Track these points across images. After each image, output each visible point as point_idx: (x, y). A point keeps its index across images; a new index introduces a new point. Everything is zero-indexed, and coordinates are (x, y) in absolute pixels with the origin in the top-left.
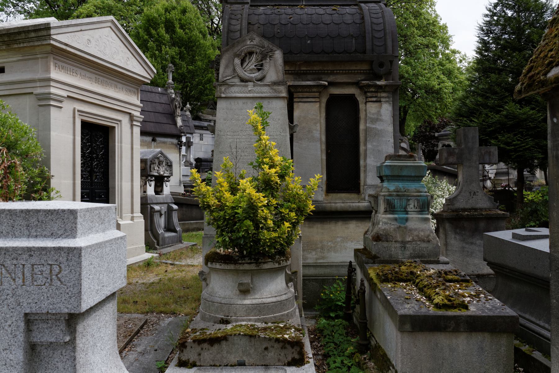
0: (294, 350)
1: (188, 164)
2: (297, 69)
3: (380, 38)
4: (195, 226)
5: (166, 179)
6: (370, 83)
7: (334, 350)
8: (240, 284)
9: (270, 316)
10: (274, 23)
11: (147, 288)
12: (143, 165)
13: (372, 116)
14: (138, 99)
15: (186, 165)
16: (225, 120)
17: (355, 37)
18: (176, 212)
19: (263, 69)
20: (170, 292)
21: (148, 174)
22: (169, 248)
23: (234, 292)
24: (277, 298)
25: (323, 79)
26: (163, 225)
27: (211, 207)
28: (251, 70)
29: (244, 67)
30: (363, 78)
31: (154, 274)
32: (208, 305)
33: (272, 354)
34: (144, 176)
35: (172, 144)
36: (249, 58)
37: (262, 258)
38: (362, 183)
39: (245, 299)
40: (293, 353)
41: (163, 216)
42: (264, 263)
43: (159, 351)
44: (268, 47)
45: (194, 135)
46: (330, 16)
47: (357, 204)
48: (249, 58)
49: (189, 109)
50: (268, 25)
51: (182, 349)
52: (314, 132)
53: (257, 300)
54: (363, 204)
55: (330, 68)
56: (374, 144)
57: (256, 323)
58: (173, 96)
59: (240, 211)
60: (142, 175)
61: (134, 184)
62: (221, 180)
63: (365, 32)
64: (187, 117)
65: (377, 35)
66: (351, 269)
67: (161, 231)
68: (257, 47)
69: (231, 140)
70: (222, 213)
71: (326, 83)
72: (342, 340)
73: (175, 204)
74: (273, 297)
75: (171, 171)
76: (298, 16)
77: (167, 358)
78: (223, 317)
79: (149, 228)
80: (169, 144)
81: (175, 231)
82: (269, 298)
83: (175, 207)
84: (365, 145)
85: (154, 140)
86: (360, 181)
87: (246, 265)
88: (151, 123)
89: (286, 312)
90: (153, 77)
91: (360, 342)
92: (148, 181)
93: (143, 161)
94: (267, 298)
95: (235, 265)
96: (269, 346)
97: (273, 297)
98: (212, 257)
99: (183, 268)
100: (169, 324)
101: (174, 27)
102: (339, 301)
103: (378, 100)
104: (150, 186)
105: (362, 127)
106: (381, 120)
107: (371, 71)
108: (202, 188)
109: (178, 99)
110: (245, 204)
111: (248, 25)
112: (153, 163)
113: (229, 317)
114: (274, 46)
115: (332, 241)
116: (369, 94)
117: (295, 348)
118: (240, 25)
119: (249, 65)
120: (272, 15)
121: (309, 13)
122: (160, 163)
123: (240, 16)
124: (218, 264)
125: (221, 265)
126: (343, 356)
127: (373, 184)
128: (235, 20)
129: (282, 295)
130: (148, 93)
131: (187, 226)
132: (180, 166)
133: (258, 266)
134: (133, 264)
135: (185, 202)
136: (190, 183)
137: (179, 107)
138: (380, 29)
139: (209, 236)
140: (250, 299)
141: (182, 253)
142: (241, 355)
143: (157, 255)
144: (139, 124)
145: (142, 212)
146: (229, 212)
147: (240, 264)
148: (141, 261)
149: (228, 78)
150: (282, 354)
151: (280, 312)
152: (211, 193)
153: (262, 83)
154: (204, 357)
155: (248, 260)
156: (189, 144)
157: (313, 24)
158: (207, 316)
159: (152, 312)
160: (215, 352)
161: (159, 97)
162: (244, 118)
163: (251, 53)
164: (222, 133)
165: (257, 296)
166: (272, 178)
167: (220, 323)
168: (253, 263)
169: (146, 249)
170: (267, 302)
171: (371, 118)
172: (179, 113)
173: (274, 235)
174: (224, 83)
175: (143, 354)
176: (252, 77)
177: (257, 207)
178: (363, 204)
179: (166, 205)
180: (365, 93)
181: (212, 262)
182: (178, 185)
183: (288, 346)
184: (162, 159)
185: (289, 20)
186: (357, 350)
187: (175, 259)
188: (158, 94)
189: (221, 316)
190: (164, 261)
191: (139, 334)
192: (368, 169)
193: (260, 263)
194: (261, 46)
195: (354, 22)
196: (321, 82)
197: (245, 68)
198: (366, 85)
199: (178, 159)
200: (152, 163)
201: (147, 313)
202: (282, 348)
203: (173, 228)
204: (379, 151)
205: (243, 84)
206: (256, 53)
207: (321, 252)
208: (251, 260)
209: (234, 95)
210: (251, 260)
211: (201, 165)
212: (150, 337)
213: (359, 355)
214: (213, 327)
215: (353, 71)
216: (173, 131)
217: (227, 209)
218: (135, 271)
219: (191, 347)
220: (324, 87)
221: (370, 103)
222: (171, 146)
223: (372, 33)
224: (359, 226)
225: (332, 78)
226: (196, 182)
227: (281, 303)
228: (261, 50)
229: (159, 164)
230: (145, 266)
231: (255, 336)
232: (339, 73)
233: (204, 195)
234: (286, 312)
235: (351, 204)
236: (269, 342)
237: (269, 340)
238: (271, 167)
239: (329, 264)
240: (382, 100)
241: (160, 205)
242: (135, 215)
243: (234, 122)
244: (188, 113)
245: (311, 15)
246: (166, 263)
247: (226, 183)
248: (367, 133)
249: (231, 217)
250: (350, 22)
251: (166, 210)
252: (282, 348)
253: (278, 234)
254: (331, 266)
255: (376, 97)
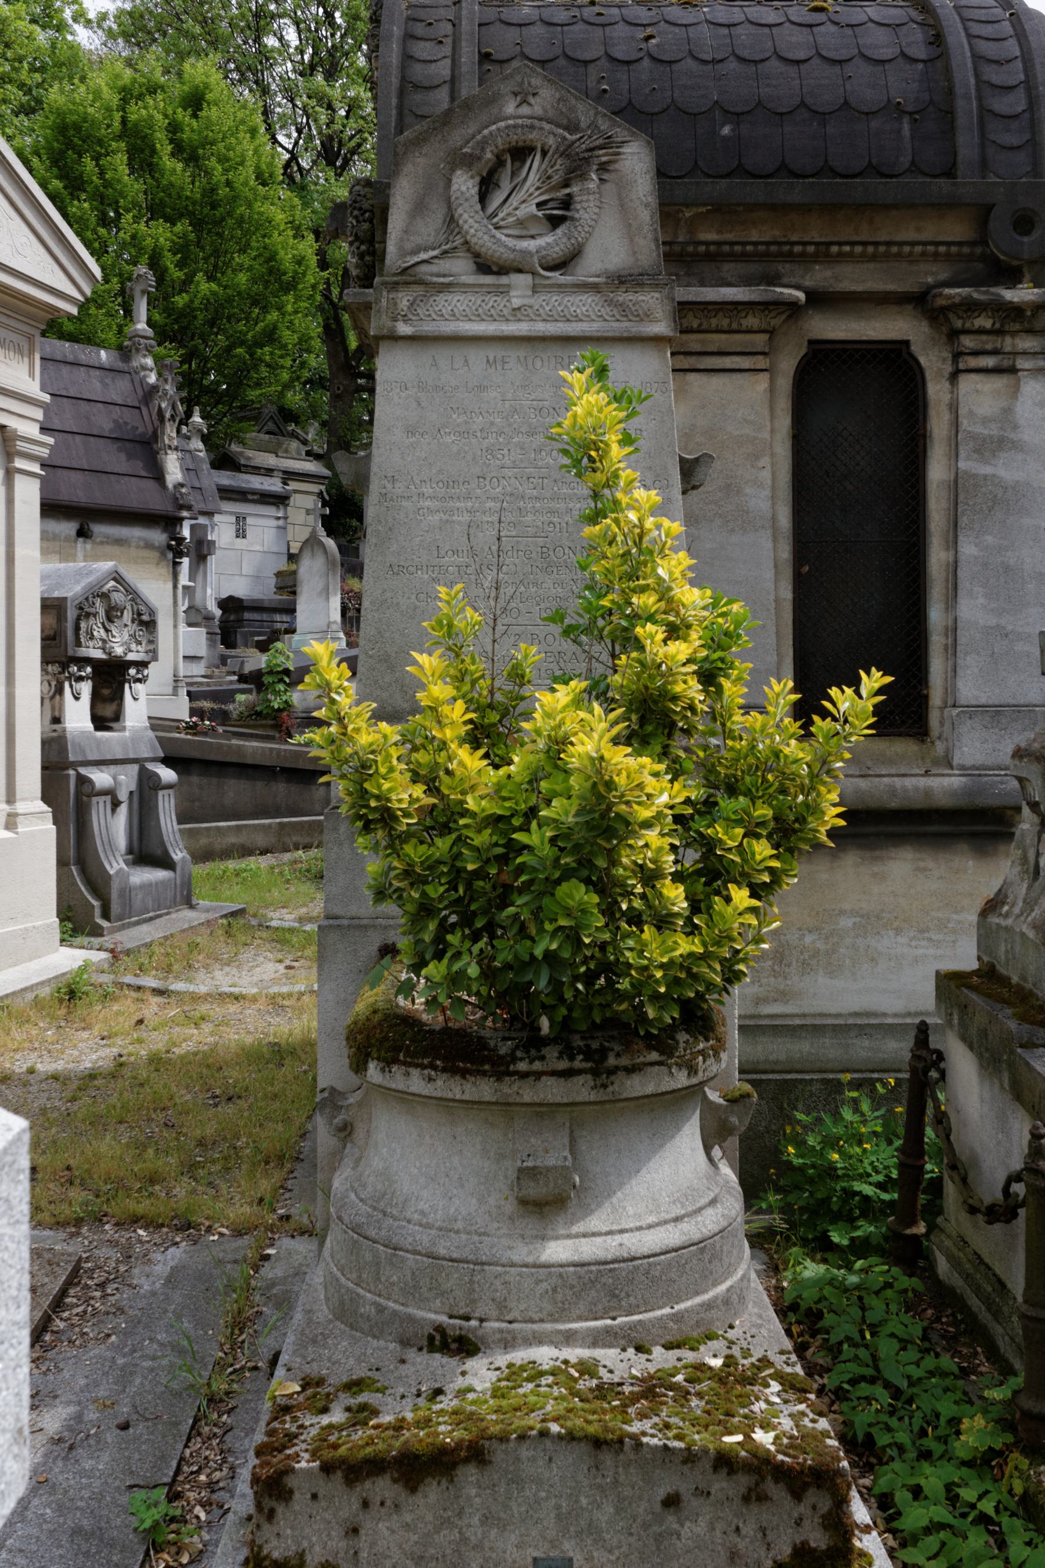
0: (803, 1509)
1: (199, 619)
2: (681, 239)
3: (1016, 117)
4: (232, 840)
5: (132, 671)
6: (975, 295)
7: (894, 1422)
8: (527, 1174)
9: (659, 1313)
10: (587, 56)
11: (73, 1100)
12: (52, 620)
13: (978, 429)
14: (31, 374)
15: (193, 620)
16: (410, 431)
17: (911, 114)
18: (171, 791)
19: (573, 219)
20: (160, 1117)
21: (70, 653)
22: (145, 928)
23: (492, 1201)
24: (684, 1226)
25: (785, 280)
26: (121, 841)
27: (396, 819)
28: (521, 223)
29: (490, 210)
30: (943, 276)
31: (96, 1031)
32: (368, 1257)
33: (701, 1528)
34: (53, 663)
35: (149, 546)
36: (514, 174)
37: (617, 1048)
38: (936, 697)
39: (544, 1238)
40: (799, 1522)
41: (123, 809)
42: (630, 1070)
43: (139, 1429)
44: (593, 125)
45: (217, 518)
46: (806, 30)
47: (923, 782)
48: (514, 174)
49: (200, 431)
50: (562, 62)
51: (268, 1503)
52: (748, 491)
53: (599, 1240)
54: (946, 781)
55: (816, 232)
56: (989, 539)
57: (599, 1353)
58: (152, 379)
59: (535, 838)
60: (46, 660)
61: (19, 692)
62: (440, 691)
63: (950, 91)
64: (194, 458)
65: (1002, 104)
66: (924, 1053)
67: (116, 865)
68: (547, 127)
69: (437, 517)
70: (443, 844)
71: (801, 296)
72: (916, 1373)
73: (168, 761)
74: (666, 1222)
75: (150, 642)
76: (677, 30)
77: (174, 1463)
78: (443, 1319)
79: (72, 853)
80: (138, 547)
81: (165, 862)
82: (650, 1227)
83: (167, 774)
84: (953, 542)
85: (82, 533)
86: (927, 687)
87: (550, 1081)
88: (72, 473)
89: (722, 1288)
90: (88, 292)
91: (1028, 1403)
92: (69, 679)
93: (51, 607)
94: (639, 1229)
95: (499, 1080)
96: (685, 1489)
97: (666, 1222)
98: (386, 1039)
99: (204, 1008)
100: (171, 1280)
101: (154, 151)
102: (864, 1176)
103: (1006, 363)
104: (77, 698)
105: (937, 472)
106: (1017, 446)
107: (979, 250)
108: (357, 730)
109: (170, 388)
110: (574, 806)
111: (480, 63)
112: (88, 615)
113: (474, 1323)
114: (615, 124)
115: (818, 929)
116: (968, 342)
117: (812, 1496)
118: (448, 61)
119: (514, 201)
120: (576, 28)
121: (721, 21)
122: (112, 614)
123: (449, 26)
124: (415, 1072)
125: (430, 1079)
126: (947, 1456)
127: (983, 700)
128: (428, 44)
129: (700, 1210)
130: (62, 366)
131: (204, 841)
132: (175, 626)
133: (604, 1086)
134: (14, 993)
135: (196, 754)
136: (208, 684)
137: (173, 418)
138: (1011, 82)
139: (345, 922)
140: (569, 1236)
141: (194, 946)
142: (551, 1534)
143: (103, 955)
144: (36, 468)
145: (46, 798)
146: (482, 839)
147: (524, 1075)
148: (42, 983)
149: (423, 256)
150: (749, 1529)
151: (697, 1293)
152: (394, 753)
153: (568, 279)
154: (373, 1544)
155: (560, 1057)
156: (202, 551)
157: (742, 60)
158: (366, 1309)
159: (99, 1219)
160: (429, 1517)
161: (102, 382)
162: (492, 424)
163: (521, 153)
164: (399, 489)
165: (595, 1222)
166: (675, 682)
167: (432, 1348)
168: (579, 1072)
169: (63, 933)
170: (646, 1251)
171: (973, 437)
172: (171, 438)
173: (685, 946)
174: (408, 278)
175: (71, 1448)
176: (525, 253)
177: (628, 823)
178: (946, 781)
179: (135, 768)
180: (954, 335)
181: (388, 1063)
182: (170, 690)
183: (775, 1490)
184: (118, 598)
185: (643, 45)
186: (1009, 1438)
187: (168, 970)
188: (98, 372)
189: (432, 1316)
190: (129, 979)
191: (48, 1337)
192: (962, 640)
193: (613, 1071)
194: (565, 122)
195: (903, 54)
196: (779, 290)
197: (494, 215)
198: (961, 304)
199: (171, 601)
200: (84, 613)
201: (79, 1222)
202: (746, 1499)
203: (159, 852)
204: (1007, 569)
205: (489, 279)
206: (544, 153)
207: (775, 974)
208: (572, 1058)
209: (449, 328)
210: (572, 1058)
211: (240, 621)
212: (96, 1351)
213: (1024, 1463)
214: (404, 1369)
215: (907, 249)
216: (153, 501)
217: (466, 826)
218: (23, 1020)
219: (314, 1496)
220: (793, 308)
221: (973, 377)
222: (146, 553)
223: (980, 99)
224: (925, 869)
225: (820, 277)
226: (333, 701)
227: (702, 1251)
228: (564, 138)
229: (110, 619)
230: (61, 1001)
231: (621, 1441)
232: (851, 254)
233: (364, 766)
234: (722, 1288)
235: (898, 782)
236: (686, 1469)
237: (685, 1462)
238: (674, 632)
239: (808, 1021)
240: (1022, 363)
241: (113, 768)
242: (20, 807)
243: (449, 439)
244: (197, 444)
245: (729, 26)
246: (139, 988)
247: (460, 705)
248: (961, 498)
249: (488, 861)
250: (887, 53)
251: (133, 787)
252: (746, 1499)
253: (704, 944)
254: (817, 1030)
255: (995, 352)
